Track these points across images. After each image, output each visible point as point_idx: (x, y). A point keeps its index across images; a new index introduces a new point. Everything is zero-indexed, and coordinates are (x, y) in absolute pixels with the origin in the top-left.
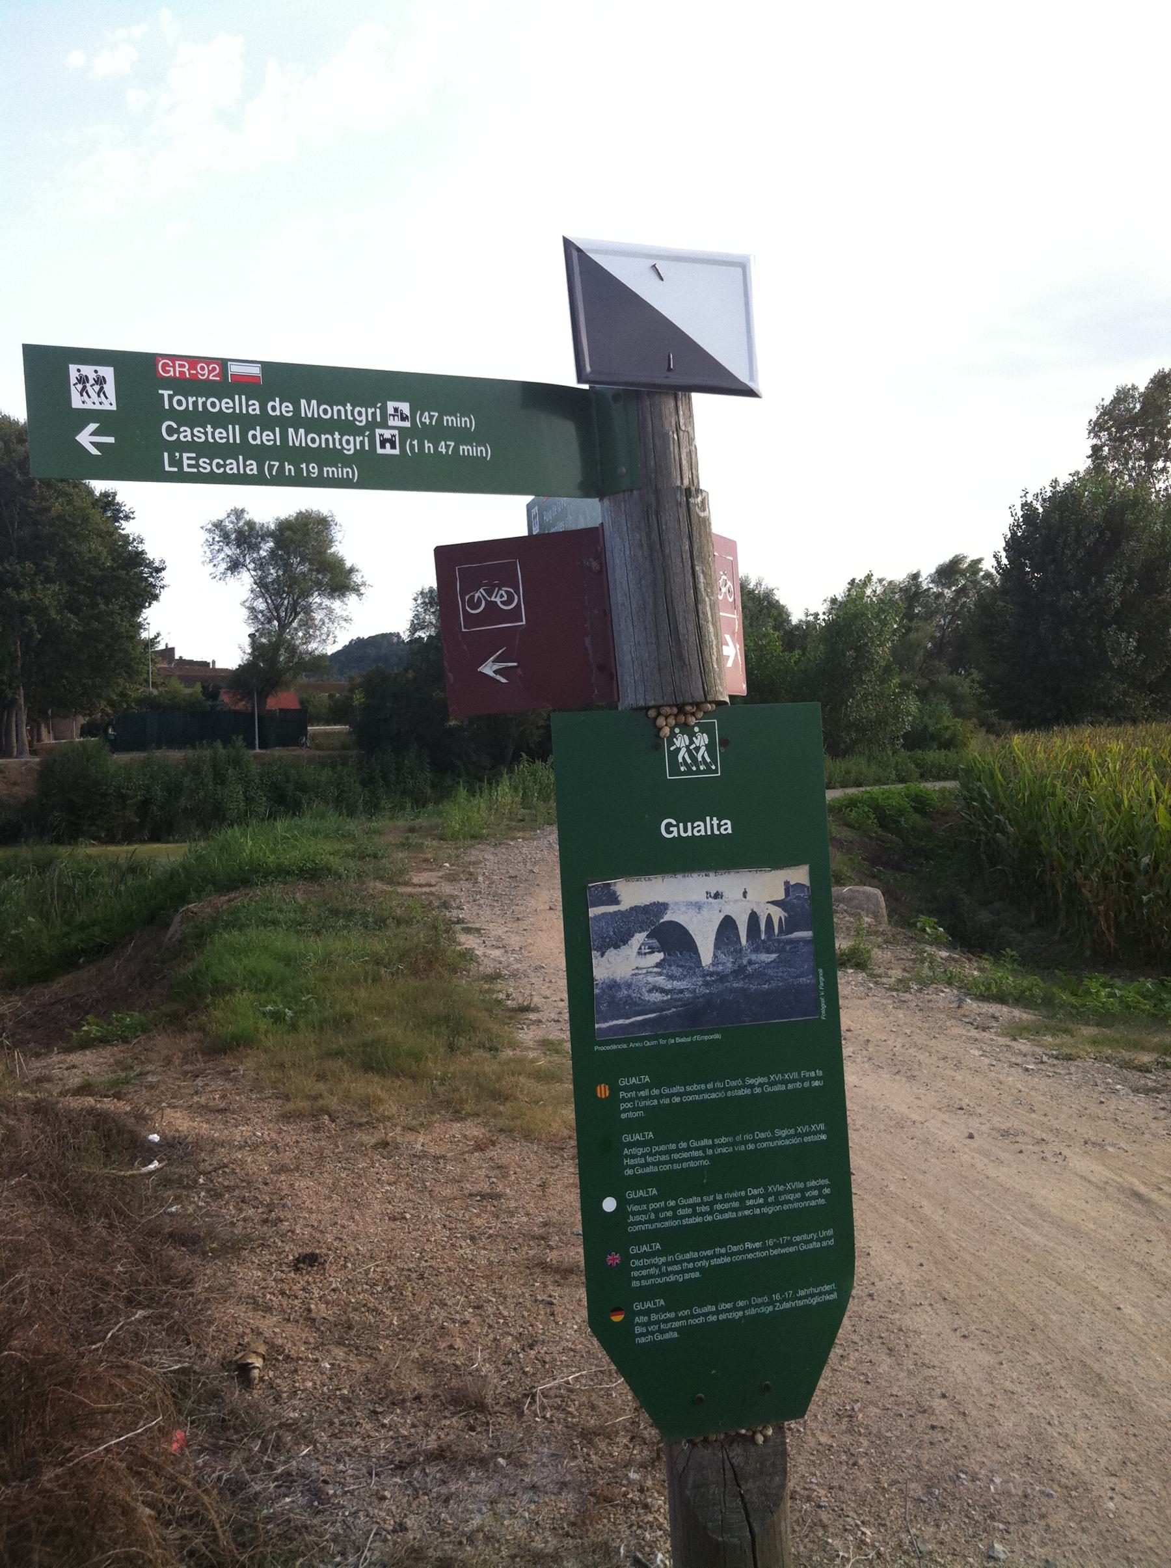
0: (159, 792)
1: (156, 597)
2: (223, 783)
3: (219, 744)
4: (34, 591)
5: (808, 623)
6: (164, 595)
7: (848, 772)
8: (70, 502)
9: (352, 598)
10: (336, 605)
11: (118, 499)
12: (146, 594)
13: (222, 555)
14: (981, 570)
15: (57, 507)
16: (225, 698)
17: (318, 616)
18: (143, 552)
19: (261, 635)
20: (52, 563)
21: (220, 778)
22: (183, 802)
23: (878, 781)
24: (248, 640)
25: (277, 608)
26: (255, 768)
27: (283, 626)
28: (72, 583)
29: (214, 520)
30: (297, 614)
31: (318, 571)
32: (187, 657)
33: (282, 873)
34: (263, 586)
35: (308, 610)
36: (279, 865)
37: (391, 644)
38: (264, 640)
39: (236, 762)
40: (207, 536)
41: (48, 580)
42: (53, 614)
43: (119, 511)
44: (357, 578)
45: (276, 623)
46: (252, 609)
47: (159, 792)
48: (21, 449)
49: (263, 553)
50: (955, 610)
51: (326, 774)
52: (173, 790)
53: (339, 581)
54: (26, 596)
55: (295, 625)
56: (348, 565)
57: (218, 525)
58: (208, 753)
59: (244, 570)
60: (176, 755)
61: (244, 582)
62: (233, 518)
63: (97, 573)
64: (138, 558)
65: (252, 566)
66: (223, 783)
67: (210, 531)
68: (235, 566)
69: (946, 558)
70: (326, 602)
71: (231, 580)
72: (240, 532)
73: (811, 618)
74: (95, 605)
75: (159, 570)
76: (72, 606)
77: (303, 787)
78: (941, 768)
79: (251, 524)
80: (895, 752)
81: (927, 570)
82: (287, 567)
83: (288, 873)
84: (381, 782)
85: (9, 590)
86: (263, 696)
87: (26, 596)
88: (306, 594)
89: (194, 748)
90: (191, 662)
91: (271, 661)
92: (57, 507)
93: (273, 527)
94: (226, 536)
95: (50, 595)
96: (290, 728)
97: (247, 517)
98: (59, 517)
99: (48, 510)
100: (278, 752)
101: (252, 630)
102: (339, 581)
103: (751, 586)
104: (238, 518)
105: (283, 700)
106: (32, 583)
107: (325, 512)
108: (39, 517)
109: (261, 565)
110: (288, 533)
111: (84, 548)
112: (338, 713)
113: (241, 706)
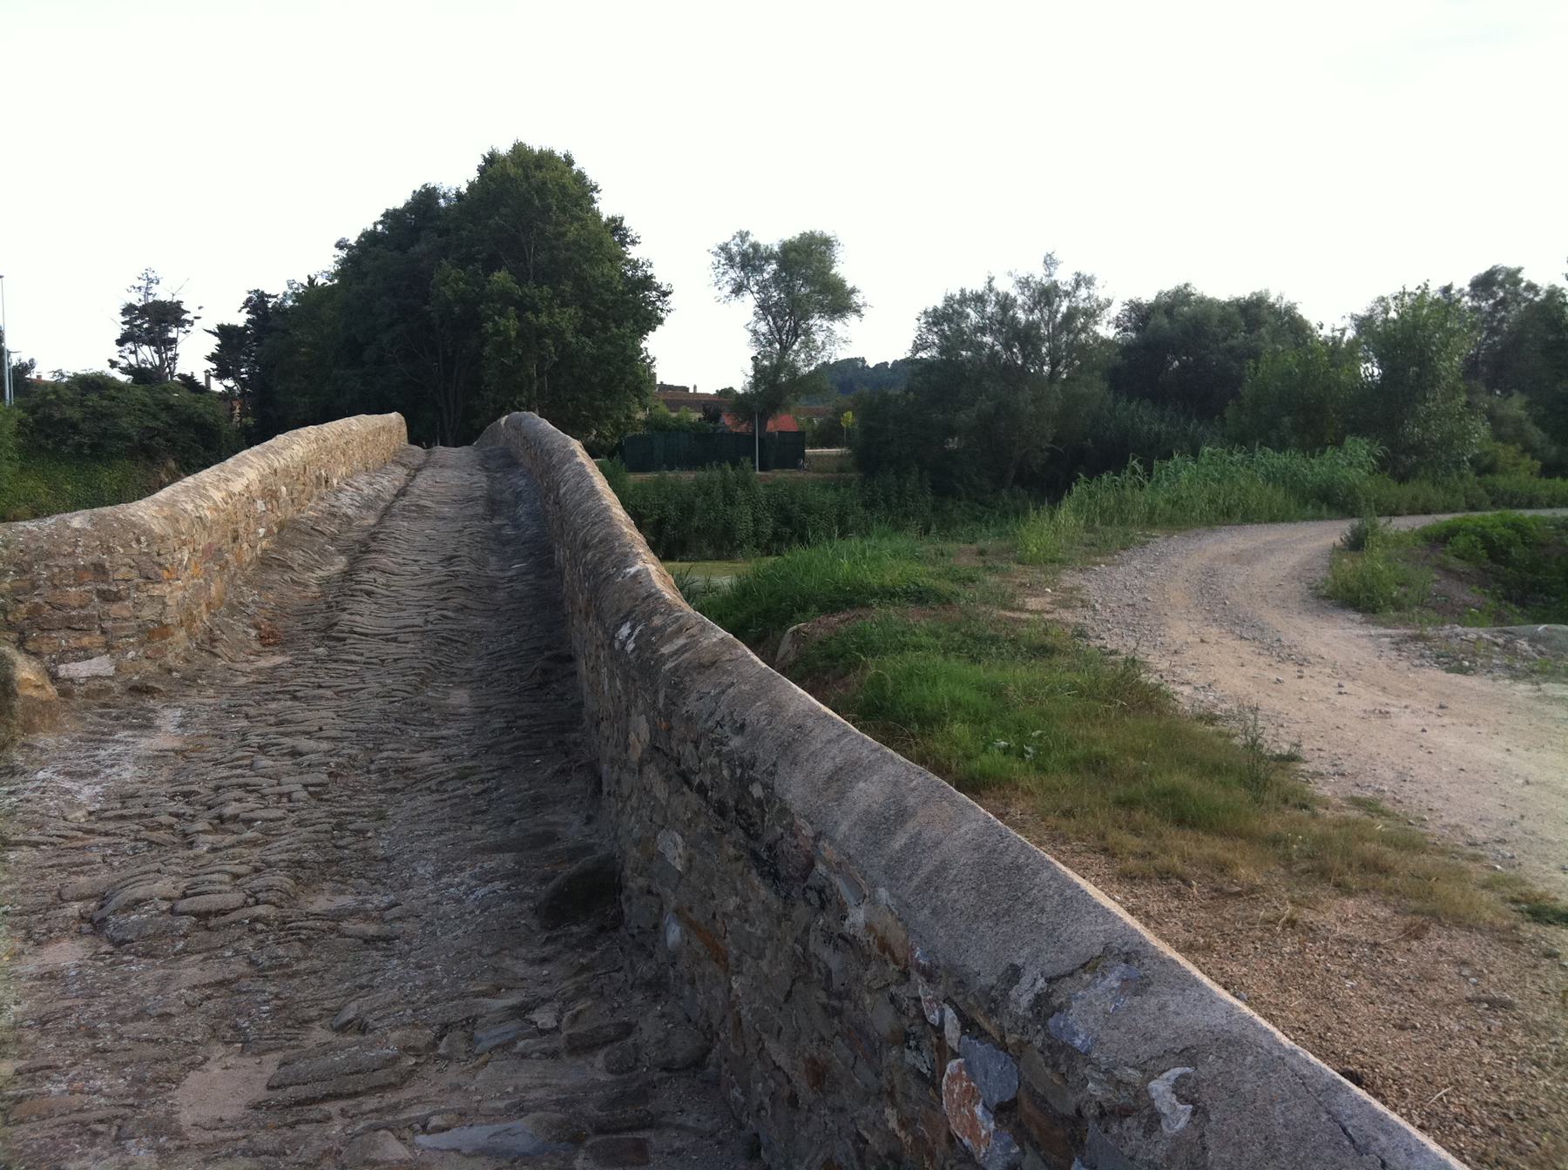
0: (672, 511)
1: (660, 321)
2: (732, 504)
3: (728, 466)
4: (551, 315)
5: (1334, 338)
6: (669, 320)
7: (1415, 498)
8: (583, 227)
9: (852, 319)
10: (837, 326)
11: (625, 224)
12: (650, 321)
13: (727, 278)
14: (1521, 280)
15: (572, 231)
16: (726, 420)
17: (819, 338)
18: (651, 277)
19: (764, 357)
20: (567, 287)
21: (730, 500)
22: (695, 522)
23: (1447, 509)
24: (751, 363)
25: (779, 330)
26: (762, 491)
27: (785, 348)
28: (584, 307)
29: (721, 243)
30: (797, 336)
31: (820, 292)
32: (667, 382)
33: (889, 594)
34: (764, 308)
35: (807, 332)
36: (882, 586)
37: (856, 369)
38: (766, 363)
39: (746, 484)
40: (715, 259)
41: (564, 304)
42: (569, 337)
43: (626, 236)
44: (857, 299)
45: (777, 346)
46: (755, 332)
47: (672, 511)
48: (539, 174)
49: (766, 276)
50: (1488, 323)
51: (829, 497)
52: (687, 510)
53: (839, 301)
54: (544, 319)
55: (795, 348)
56: (849, 285)
57: (724, 248)
58: (716, 474)
59: (747, 293)
60: (687, 477)
61: (749, 301)
62: (738, 240)
63: (608, 297)
64: (647, 283)
65: (755, 289)
66: (732, 504)
67: (716, 254)
68: (738, 289)
69: (1482, 269)
70: (826, 324)
71: (736, 302)
72: (744, 255)
73: (1338, 334)
74: (606, 329)
75: (665, 294)
76: (585, 330)
77: (808, 510)
78: (1513, 496)
79: (755, 247)
80: (1461, 477)
81: (1462, 282)
82: (789, 290)
83: (893, 595)
84: (883, 505)
85: (529, 314)
86: (764, 418)
87: (544, 319)
88: (806, 316)
89: (703, 467)
90: (671, 387)
91: (774, 383)
92: (572, 231)
93: (776, 249)
94: (730, 258)
95: (567, 318)
96: (787, 452)
97: (752, 239)
98: (575, 242)
99: (564, 235)
100: (779, 475)
101: (754, 353)
102: (839, 301)
103: (1271, 300)
104: (743, 241)
105: (782, 423)
106: (550, 307)
107: (828, 233)
108: (554, 243)
109: (763, 287)
110: (793, 255)
111: (597, 273)
112: (829, 435)
113: (743, 428)
